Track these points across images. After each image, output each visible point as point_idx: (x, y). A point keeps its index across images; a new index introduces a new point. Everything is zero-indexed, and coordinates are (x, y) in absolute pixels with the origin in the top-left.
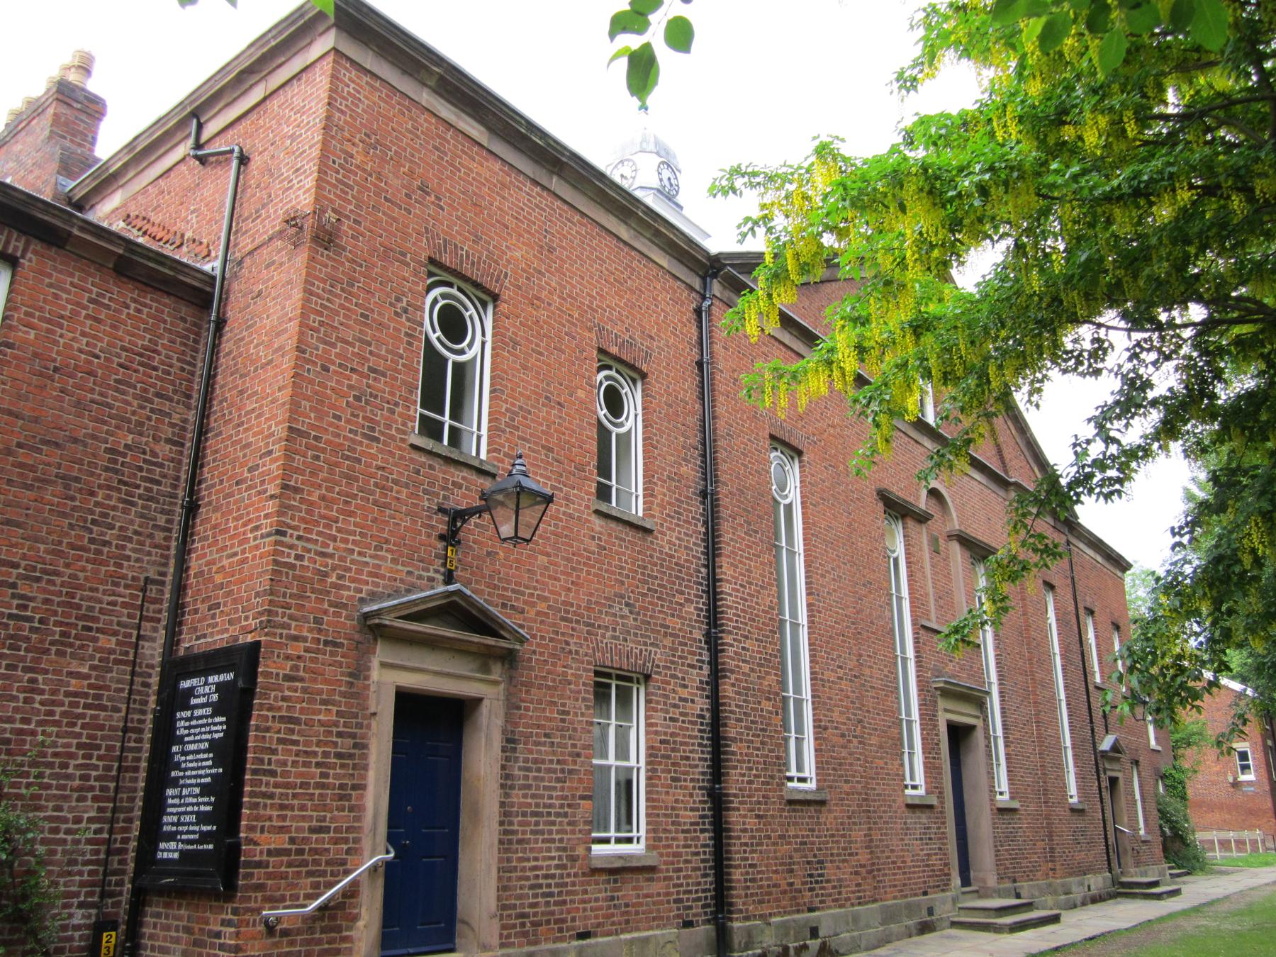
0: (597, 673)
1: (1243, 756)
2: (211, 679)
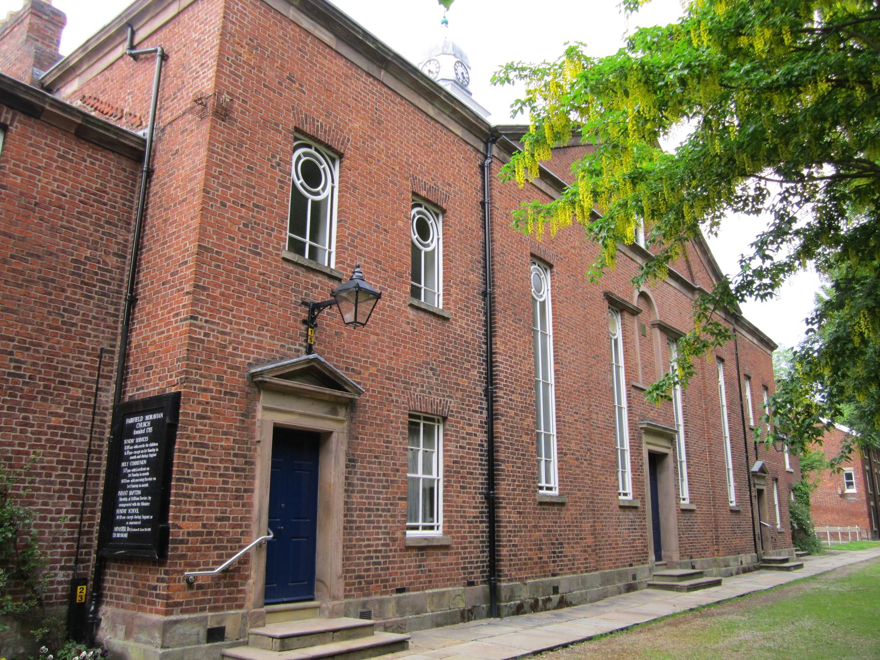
0: (411, 416)
1: (849, 476)
2: (147, 418)
